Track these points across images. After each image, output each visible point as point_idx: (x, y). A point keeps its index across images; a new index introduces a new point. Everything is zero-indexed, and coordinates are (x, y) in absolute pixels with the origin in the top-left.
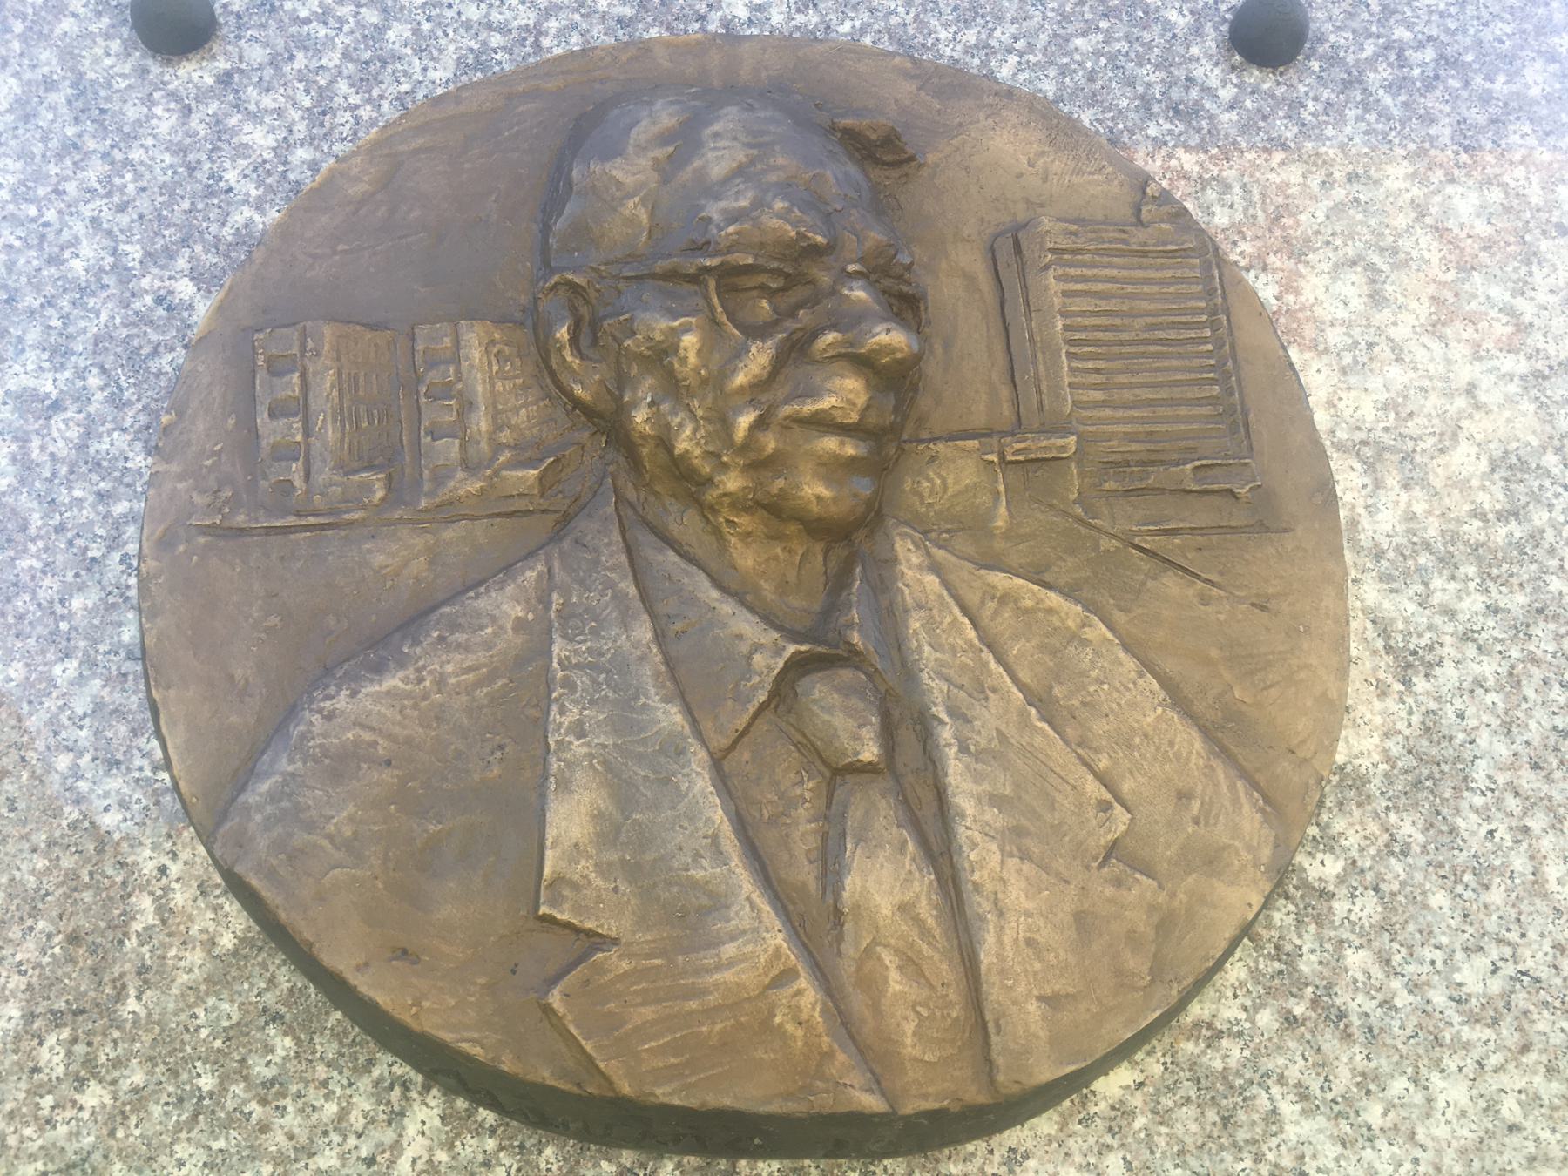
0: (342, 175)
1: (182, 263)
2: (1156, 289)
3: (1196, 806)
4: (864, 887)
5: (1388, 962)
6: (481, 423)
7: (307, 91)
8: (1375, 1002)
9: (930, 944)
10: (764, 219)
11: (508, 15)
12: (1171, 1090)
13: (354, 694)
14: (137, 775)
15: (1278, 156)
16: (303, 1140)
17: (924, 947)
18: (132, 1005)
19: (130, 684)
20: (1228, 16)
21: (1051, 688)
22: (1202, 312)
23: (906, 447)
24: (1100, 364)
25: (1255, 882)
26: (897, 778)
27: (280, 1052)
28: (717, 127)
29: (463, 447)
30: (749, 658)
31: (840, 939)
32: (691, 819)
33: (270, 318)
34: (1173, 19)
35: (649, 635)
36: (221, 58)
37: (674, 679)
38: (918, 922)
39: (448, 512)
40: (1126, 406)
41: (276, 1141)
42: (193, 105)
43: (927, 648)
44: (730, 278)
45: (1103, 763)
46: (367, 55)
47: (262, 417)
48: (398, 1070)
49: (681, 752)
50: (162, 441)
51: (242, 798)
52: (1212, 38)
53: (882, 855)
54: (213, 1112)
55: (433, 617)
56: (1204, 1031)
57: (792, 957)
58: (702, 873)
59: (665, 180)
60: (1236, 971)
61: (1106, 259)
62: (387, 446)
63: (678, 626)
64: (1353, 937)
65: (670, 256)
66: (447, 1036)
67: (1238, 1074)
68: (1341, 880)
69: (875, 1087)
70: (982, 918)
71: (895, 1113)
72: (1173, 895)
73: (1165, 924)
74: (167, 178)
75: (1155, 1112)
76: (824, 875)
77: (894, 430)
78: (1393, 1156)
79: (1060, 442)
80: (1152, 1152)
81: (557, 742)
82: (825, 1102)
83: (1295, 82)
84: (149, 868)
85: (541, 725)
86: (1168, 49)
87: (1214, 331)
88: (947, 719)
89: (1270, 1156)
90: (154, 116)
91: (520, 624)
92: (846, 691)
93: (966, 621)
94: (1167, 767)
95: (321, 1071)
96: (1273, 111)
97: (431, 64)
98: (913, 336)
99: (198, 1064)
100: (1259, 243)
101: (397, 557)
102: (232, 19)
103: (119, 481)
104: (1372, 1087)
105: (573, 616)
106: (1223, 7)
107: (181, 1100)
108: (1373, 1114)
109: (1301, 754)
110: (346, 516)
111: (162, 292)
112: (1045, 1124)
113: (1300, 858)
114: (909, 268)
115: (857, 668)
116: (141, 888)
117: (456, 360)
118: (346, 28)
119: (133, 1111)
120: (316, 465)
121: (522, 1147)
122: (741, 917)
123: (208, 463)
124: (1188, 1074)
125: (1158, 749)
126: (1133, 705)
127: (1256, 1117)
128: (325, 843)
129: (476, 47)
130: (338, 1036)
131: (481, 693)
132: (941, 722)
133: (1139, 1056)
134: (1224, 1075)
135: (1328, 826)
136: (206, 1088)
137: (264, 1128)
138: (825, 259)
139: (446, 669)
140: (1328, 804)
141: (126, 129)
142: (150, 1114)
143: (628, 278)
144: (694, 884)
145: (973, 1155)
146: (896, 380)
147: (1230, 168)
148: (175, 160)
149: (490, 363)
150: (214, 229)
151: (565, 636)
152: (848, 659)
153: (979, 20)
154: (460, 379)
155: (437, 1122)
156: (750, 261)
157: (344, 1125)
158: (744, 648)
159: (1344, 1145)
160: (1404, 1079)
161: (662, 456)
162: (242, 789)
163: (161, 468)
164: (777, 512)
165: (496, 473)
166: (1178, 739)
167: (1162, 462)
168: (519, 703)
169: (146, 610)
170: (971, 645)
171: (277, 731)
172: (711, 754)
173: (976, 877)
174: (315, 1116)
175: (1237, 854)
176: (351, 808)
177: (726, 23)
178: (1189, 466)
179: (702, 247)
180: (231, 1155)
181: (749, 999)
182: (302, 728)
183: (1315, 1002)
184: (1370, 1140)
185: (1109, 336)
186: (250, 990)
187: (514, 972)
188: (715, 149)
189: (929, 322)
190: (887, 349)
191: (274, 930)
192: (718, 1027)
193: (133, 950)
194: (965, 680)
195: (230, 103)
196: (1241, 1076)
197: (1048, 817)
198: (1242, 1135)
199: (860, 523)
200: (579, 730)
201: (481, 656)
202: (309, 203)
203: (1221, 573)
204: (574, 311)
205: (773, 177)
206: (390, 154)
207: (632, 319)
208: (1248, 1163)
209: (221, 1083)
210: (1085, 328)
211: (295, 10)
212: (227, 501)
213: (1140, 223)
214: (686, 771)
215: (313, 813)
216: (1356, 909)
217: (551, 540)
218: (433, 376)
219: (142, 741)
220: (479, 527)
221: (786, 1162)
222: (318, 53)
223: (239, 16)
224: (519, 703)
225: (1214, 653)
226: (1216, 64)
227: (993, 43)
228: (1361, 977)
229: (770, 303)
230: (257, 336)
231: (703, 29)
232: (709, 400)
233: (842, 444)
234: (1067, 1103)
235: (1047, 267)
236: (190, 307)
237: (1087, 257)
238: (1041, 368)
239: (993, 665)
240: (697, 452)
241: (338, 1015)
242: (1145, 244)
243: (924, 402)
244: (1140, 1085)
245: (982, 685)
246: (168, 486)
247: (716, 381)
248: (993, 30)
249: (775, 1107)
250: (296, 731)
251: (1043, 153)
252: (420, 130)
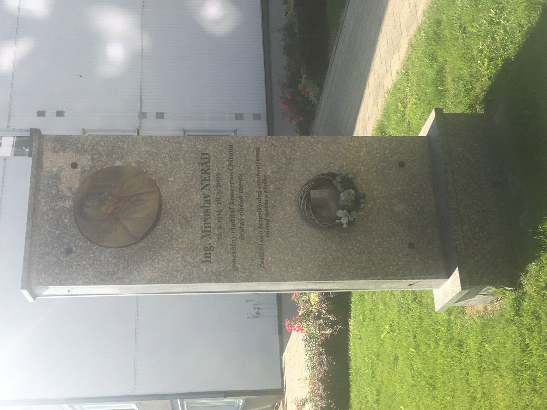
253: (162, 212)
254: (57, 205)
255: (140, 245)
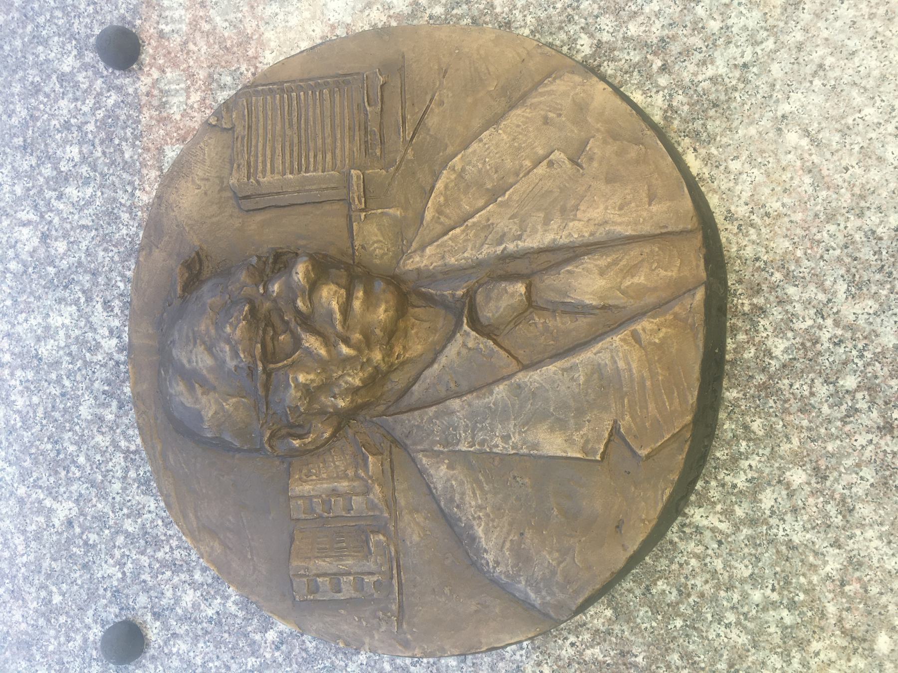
0: (210, 556)
1: (258, 637)
2: (269, 122)
3: (551, 115)
4: (591, 294)
5: (635, 13)
6: (343, 485)
7: (163, 573)
8: (657, 21)
9: (621, 260)
10: (236, 338)
11: (118, 467)
12: (698, 134)
13: (486, 551)
14: (524, 658)
15: (191, 46)
16: (708, 576)
17: (622, 263)
18: (639, 659)
19: (478, 661)
20: (110, 70)
21: (487, 189)
22: (282, 98)
23: (356, 261)
24: (312, 154)
25: (592, 86)
26: (533, 273)
27: (665, 587)
28: (185, 361)
29: (357, 495)
30: (470, 349)
31: (617, 307)
32: (554, 382)
33: (294, 596)
34: (113, 102)
35: (458, 401)
36: (145, 618)
37: (480, 388)
38: (609, 266)
39: (391, 503)
40: (335, 142)
41: (708, 589)
42: (171, 632)
43: (466, 255)
44: (268, 357)
45: (528, 163)
46: (142, 542)
47: (340, 596)
48: (675, 528)
49: (519, 386)
50: (353, 646)
51: (538, 606)
52: (123, 80)
53: (574, 283)
54: (693, 620)
55: (446, 511)
56: (669, 114)
57: (626, 333)
58: (582, 377)
59: (214, 389)
60: (637, 97)
61: (253, 149)
62: (356, 533)
63: (452, 385)
64: (622, 31)
65: (256, 387)
66: (660, 506)
67: (691, 97)
68: (591, 36)
69: (692, 292)
70: (608, 233)
71: (705, 283)
72: (598, 130)
73: (614, 136)
74: (212, 645)
75: (709, 143)
76: (583, 313)
77: (348, 268)
78: (737, 16)
79: (355, 179)
80: (730, 145)
81: (513, 449)
82: (699, 318)
83: (148, 34)
84: (571, 651)
85: (503, 457)
86: (130, 105)
87: (293, 91)
88: (503, 246)
89: (734, 82)
90: (178, 652)
91: (450, 467)
92: (488, 299)
93: (451, 233)
94: (531, 129)
95: (675, 567)
96: (164, 47)
97: (146, 509)
98: (299, 260)
99: (669, 627)
100: (241, 60)
101: (415, 528)
102: (123, 612)
103: (373, 667)
104: (700, 25)
105: (446, 439)
106: (105, 73)
107: (687, 635)
108: (714, 26)
109: (524, 55)
110: (393, 554)
111: (273, 647)
112: (713, 201)
113: (579, 57)
114: (259, 258)
115: (476, 292)
116: (581, 654)
117: (310, 498)
118: (127, 553)
119: (692, 659)
120: (366, 569)
121: (715, 468)
122: (604, 358)
123: (364, 623)
124: (690, 124)
125: (520, 133)
126: (497, 146)
127: (713, 89)
128: (562, 566)
129: (136, 485)
130: (657, 558)
131: (486, 488)
132: (505, 248)
133: (680, 149)
134: (691, 105)
135: (562, 41)
136: (682, 623)
137: (702, 595)
138: (257, 305)
139: (473, 504)
140: (551, 40)
141: (185, 666)
142: (693, 651)
143: (267, 409)
144: (587, 381)
145: (727, 239)
146: (324, 267)
147: (198, 74)
148: (202, 641)
149: (312, 480)
150: (238, 621)
151: (457, 444)
152: (471, 298)
153: (115, 211)
154: (320, 496)
155: (702, 510)
156: (259, 346)
157: (701, 556)
158: (464, 351)
159: (730, 42)
160: (697, 8)
161: (363, 392)
162: (533, 606)
163: (367, 647)
164: (392, 333)
165: (371, 478)
166: (515, 122)
167: (366, 123)
168: (487, 466)
169: (441, 653)
170: (463, 231)
171: (503, 589)
172: (520, 371)
173: (586, 235)
174: (697, 570)
175: (577, 94)
176: (545, 553)
177: (120, 350)
178: (368, 108)
179: (251, 371)
180: (715, 611)
181: (646, 355)
182: (503, 577)
183: (655, 53)
184: (728, 28)
185: (296, 148)
186: (634, 602)
187: (629, 473)
188: (197, 362)
189: (288, 247)
190: (307, 274)
191: (606, 589)
192: (660, 371)
193: (612, 659)
194: (483, 235)
195: (170, 614)
196: (692, 95)
197: (556, 194)
198: (723, 97)
199: (398, 288)
200: (506, 438)
201: (467, 486)
202: (225, 572)
203: (426, 93)
204: (283, 437)
205: (213, 331)
206: (199, 532)
207: (289, 407)
208: (737, 94)
209: (679, 616)
210: (292, 162)
211: (118, 580)
212: (384, 614)
213: (232, 129)
214: (529, 384)
215: (547, 571)
216: (607, 28)
217: (406, 449)
218: (319, 510)
219: (507, 656)
220: (399, 487)
221: (728, 335)
222: (142, 567)
223: (122, 609)
224: (487, 466)
225: (470, 100)
226: (139, 79)
227: (128, 203)
228: (643, 28)
229: (280, 335)
230: (297, 599)
231: (124, 363)
232: (333, 368)
233: (357, 298)
234: (703, 189)
235: (258, 182)
236: (281, 633)
237: (252, 159)
238: (314, 187)
239: (475, 220)
240: (361, 374)
241: (647, 558)
242: (244, 127)
243: (332, 251)
244: (695, 150)
245: (485, 226)
246: (376, 643)
247: (323, 365)
248: (121, 204)
249: (701, 344)
250: (504, 579)
251: (193, 181)
252: (185, 516)
253: (731, 394)
254: (48, 332)
255: (567, 652)
